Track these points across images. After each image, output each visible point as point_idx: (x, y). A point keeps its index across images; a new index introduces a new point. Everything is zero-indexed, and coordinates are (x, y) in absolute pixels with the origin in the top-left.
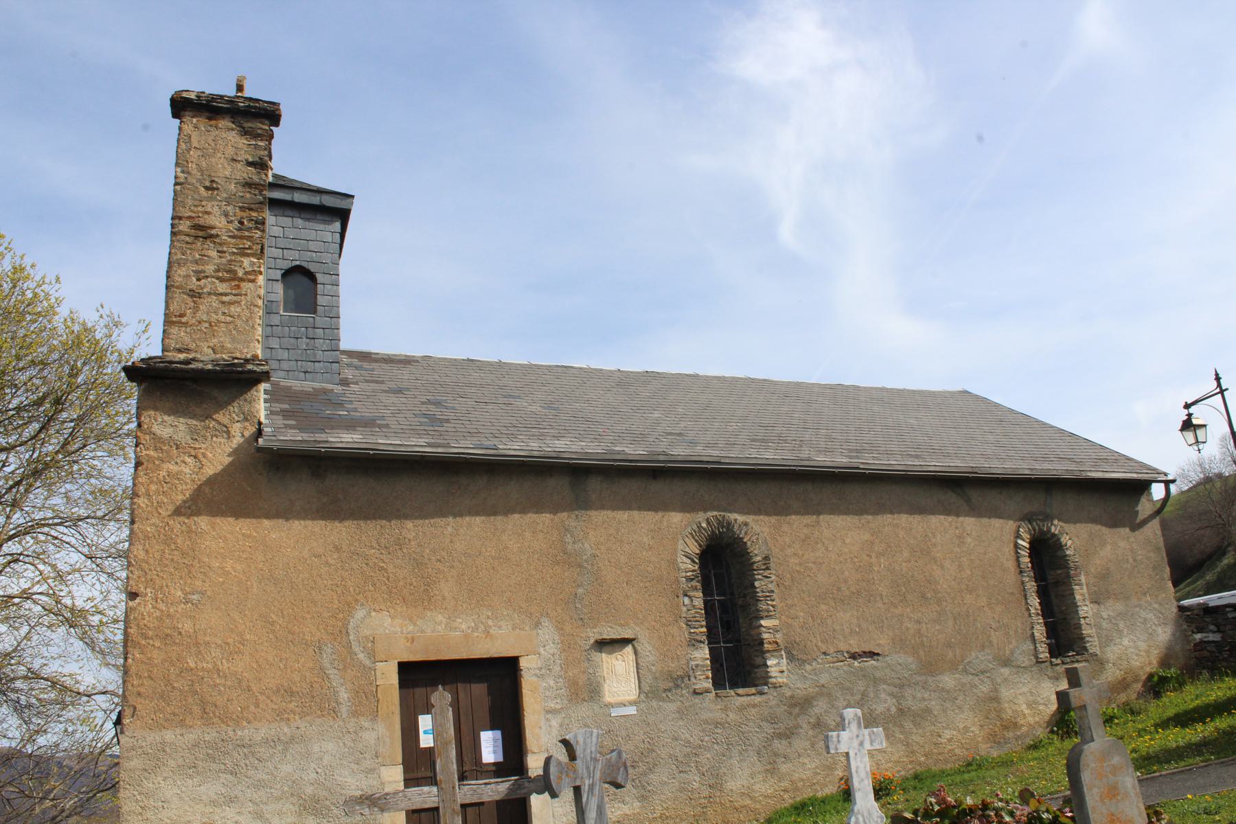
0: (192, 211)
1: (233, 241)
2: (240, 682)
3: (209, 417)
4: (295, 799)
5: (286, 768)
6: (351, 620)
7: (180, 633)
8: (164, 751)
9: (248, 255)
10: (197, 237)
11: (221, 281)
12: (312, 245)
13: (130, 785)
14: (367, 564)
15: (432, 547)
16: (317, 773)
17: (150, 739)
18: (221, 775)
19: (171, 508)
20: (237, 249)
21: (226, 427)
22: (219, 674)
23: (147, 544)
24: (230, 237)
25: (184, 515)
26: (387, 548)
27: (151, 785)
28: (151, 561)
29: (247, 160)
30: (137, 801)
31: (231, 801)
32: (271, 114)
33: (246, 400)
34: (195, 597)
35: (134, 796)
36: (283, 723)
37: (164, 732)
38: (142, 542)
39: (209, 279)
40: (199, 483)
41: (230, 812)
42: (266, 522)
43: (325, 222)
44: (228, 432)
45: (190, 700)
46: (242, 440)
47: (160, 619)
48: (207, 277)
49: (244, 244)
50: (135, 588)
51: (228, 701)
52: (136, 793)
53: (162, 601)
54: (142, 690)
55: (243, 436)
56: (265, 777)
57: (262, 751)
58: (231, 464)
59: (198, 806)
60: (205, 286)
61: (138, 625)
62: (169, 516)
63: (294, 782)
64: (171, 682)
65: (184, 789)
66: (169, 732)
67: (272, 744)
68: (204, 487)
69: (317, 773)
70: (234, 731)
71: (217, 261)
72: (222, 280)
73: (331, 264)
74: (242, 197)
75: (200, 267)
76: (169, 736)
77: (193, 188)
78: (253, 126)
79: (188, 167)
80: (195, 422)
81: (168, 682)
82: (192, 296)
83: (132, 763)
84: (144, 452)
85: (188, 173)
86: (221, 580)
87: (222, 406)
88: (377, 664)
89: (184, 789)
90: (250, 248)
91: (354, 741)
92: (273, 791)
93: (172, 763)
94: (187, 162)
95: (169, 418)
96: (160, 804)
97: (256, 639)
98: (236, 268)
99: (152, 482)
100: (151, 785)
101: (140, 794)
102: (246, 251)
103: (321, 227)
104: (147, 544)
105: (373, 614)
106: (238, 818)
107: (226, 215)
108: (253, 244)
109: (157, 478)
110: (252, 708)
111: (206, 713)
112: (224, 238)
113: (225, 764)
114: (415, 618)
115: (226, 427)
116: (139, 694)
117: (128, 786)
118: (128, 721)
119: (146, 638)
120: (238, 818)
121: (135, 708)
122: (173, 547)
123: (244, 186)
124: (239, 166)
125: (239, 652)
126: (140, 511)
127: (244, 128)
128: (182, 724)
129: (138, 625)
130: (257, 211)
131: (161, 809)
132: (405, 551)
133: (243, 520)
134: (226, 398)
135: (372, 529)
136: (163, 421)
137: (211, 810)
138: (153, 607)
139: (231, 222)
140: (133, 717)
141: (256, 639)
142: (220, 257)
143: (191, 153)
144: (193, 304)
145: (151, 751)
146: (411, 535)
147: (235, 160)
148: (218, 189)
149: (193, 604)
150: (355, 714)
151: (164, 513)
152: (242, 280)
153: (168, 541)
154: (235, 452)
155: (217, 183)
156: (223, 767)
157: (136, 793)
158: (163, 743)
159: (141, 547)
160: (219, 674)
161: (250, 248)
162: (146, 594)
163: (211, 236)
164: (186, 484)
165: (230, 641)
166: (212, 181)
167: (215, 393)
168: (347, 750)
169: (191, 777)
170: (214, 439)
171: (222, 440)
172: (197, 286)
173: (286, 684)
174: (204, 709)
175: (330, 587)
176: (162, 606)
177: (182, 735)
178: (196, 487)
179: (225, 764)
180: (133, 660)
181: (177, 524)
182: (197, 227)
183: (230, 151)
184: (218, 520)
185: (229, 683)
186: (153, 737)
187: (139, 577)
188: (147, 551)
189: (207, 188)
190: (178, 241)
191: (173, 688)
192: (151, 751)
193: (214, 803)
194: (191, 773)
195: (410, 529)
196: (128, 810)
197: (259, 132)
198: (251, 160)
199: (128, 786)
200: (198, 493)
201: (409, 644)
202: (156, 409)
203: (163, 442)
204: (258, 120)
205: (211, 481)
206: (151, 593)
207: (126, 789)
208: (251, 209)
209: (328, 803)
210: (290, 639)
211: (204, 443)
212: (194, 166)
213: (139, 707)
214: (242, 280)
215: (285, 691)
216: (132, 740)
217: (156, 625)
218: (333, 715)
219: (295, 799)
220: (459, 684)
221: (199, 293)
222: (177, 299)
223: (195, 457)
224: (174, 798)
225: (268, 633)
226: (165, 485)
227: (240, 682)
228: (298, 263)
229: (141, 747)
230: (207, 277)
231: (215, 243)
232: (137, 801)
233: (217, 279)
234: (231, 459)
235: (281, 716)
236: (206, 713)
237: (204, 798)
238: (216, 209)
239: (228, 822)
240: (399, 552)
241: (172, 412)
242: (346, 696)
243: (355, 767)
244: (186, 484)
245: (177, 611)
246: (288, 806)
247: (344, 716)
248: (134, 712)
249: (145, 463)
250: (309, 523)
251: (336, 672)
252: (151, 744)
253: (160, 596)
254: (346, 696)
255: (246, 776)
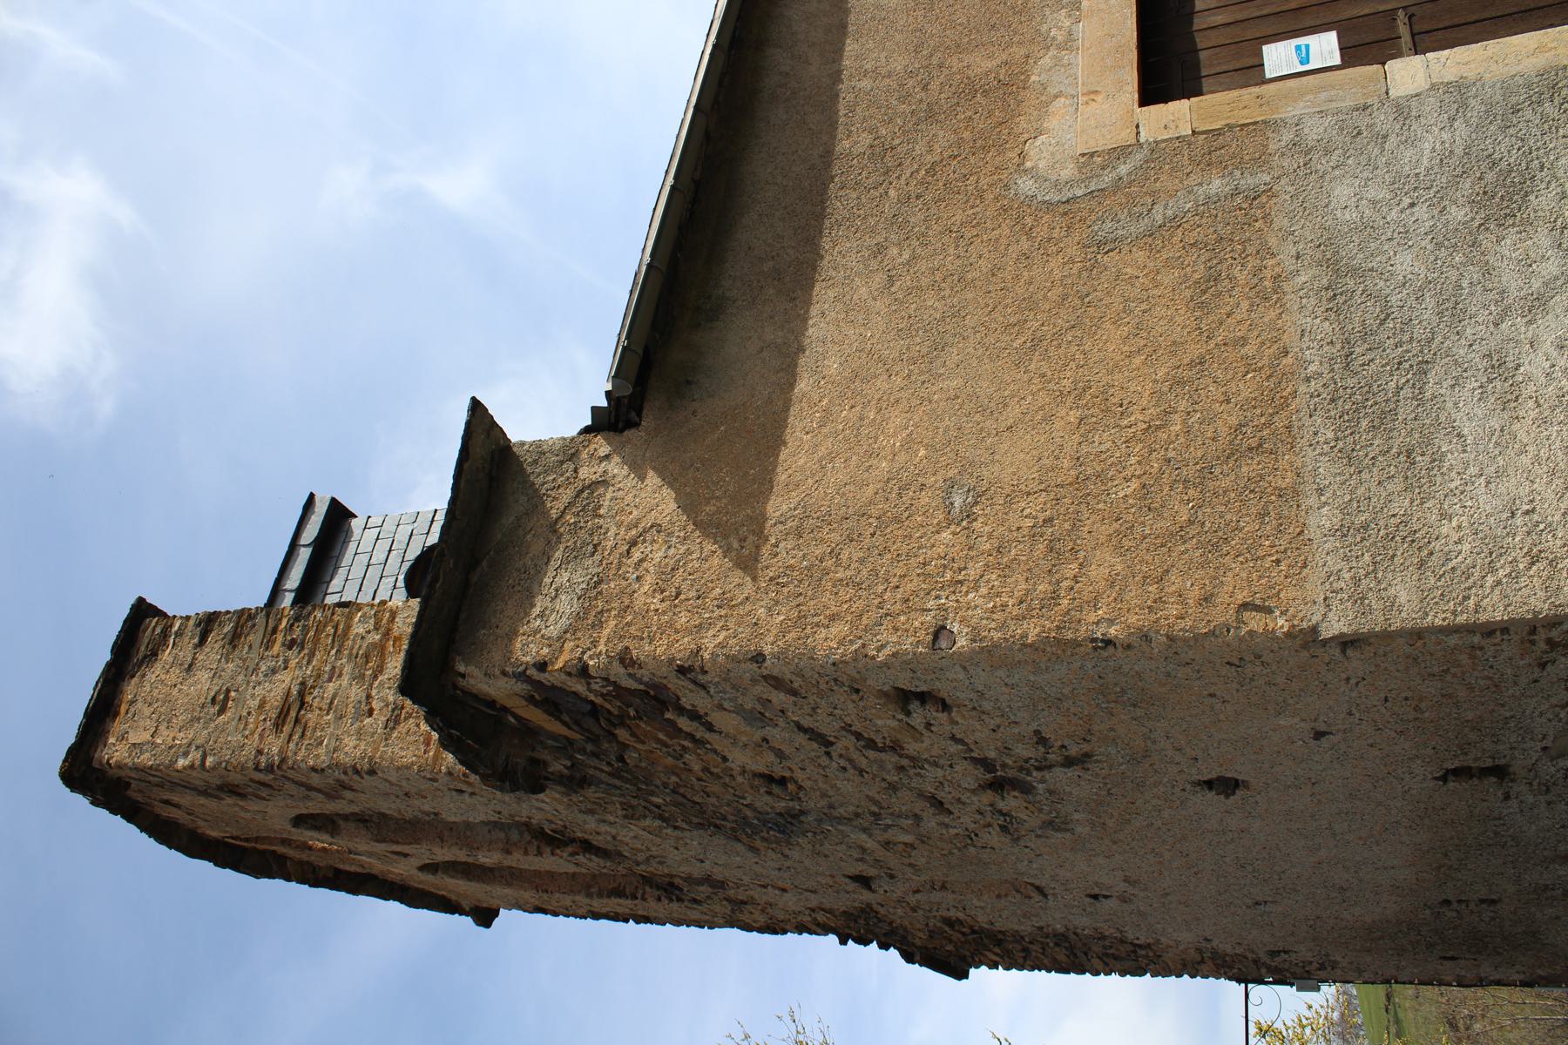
0: (252, 733)
1: (318, 655)
2: (1180, 383)
3: (553, 527)
4: (1486, 240)
5: (1405, 263)
6: (1039, 199)
7: (1049, 521)
8: (1365, 527)
9: (348, 627)
10: (297, 721)
11: (381, 672)
12: (379, 556)
13: (1466, 598)
14: (918, 197)
15: (895, 103)
16: (1412, 205)
17: (1334, 563)
18: (1428, 395)
19: (737, 576)
20: (332, 648)
21: (582, 491)
22: (1158, 428)
23: (816, 619)
24: (309, 662)
25: (758, 547)
26: (886, 173)
27: (1466, 547)
28: (858, 605)
29: (196, 646)
30: (1514, 576)
31: (1499, 366)
32: (142, 611)
33: (535, 462)
34: (958, 501)
35: (1499, 583)
36: (1286, 287)
37: (1312, 532)
38: (808, 630)
39: (374, 692)
40: (691, 527)
41: (1534, 365)
42: (802, 386)
43: (346, 542)
44: (594, 485)
45: (1226, 483)
46: (616, 459)
47: (1006, 571)
48: (369, 697)
49: (328, 635)
50: (921, 634)
51: (1228, 401)
52: (1490, 580)
53: (960, 570)
54: (1194, 594)
55: (607, 457)
56: (1430, 302)
57: (1363, 314)
58: (661, 473)
59: (1522, 435)
60: (382, 699)
61: (1020, 618)
62: (754, 579)
63: (1439, 245)
64: (1177, 528)
65: (1473, 470)
66: (1312, 521)
67: (1340, 300)
68: (703, 517)
69: (1412, 205)
70: (1308, 380)
71: (345, 681)
72: (380, 670)
73: (415, 525)
74: (250, 647)
75: (351, 710)
76: (1322, 519)
77: (216, 734)
78: (146, 641)
79: (180, 745)
80: (558, 554)
81: (1179, 534)
82: (397, 722)
83: (1403, 597)
84: (602, 648)
85: (190, 744)
86: (922, 453)
87: (536, 501)
88: (1142, 140)
89: (1473, 470)
90: (336, 628)
91: (1327, 152)
92: (1465, 284)
93: (1400, 505)
94: (171, 748)
95: (539, 604)
96: (1519, 521)
97: (1073, 365)
98: (365, 645)
99: (670, 624)
100: (1466, 547)
101: (1493, 571)
102: (340, 631)
103: (352, 547)
104: (816, 619)
105: (1028, 164)
106: (1547, 346)
107: (274, 671)
108: (331, 620)
109: (664, 613)
110: (1248, 350)
111: (1260, 445)
112: (308, 672)
113: (1399, 389)
114: (1043, 98)
115: (582, 491)
116: (1207, 599)
117: (1471, 602)
118: (1281, 622)
119: (1055, 596)
120: (1547, 346)
121: (1245, 606)
122: (829, 563)
123: (235, 647)
124: (200, 657)
125: (1105, 395)
126: (732, 642)
127: (145, 657)
128: (1291, 494)
129: (1020, 618)
130: (280, 620)
131: (1536, 517)
132: (897, 141)
133: (788, 431)
134: (523, 499)
135: (841, 202)
136: (541, 615)
137: (1531, 403)
138: (976, 588)
139: (286, 661)
140: (1269, 611)
141: (1073, 365)
142: (340, 675)
143: (159, 741)
144: (411, 720)
145: (1367, 557)
146: (866, 139)
147: (190, 666)
148: (228, 691)
149: (976, 503)
150: (1261, 160)
151: (749, 587)
152: (387, 634)
153: (815, 575)
154: (638, 470)
155: (217, 693)
156: (1406, 392)
157: (1490, 580)
158: (1342, 532)
159: (823, 633)
160: (1158, 428)
161: (336, 628)
162: (940, 608)
163: (301, 694)
164: (689, 552)
165: (1073, 416)
166: (214, 700)
167: (508, 520)
168: (1350, 162)
169: (1438, 459)
170: (602, 511)
171: (609, 496)
172: (380, 714)
173: (1188, 293)
174: (1250, 449)
175: (961, 251)
176: (973, 572)
177: (1320, 491)
178: (698, 533)
179: (1399, 389)
180: (1111, 622)
181: (781, 554)
182: (278, 725)
183: (175, 675)
184: (782, 477)
185: (1183, 405)
186: (1327, 556)
187: (896, 629)
188: (833, 618)
189: (222, 711)
190: (296, 753)
191: (1190, 522)
192: (1367, 557)
193: (1509, 401)
194: (1427, 458)
195: (852, 142)
196: (1541, 594)
197: (158, 630)
198: (196, 640)
199: (1471, 602)
200: (710, 528)
201: (1099, 98)
202: (514, 633)
203: (587, 611)
204: (141, 635)
205: (688, 505)
206: (938, 597)
207: (1477, 605)
208: (275, 630)
209: (1490, 177)
210: (1077, 302)
211: (608, 530)
212: (182, 735)
213: (1241, 597)
214: (387, 634)
215: (1204, 292)
216: (1335, 603)
217: (1021, 579)
218: (1264, 199)
219: (1486, 240)
220: (1195, 28)
221: (393, 710)
222: (396, 750)
223: (633, 543)
224: (1502, 489)
225: (1059, 346)
226: (682, 597)
227: (1180, 383)
228: (401, 577)
229: (1356, 581)
230: (369, 697)
231: (313, 687)
232: (1514, 576)
233: (376, 677)
234: (651, 473)
235: (1270, 293)
236: (1260, 445)
237: (1495, 423)
238: (259, 691)
239: (1562, 362)
240: (899, 149)
241: (528, 598)
242: (1217, 183)
243: (1393, 141)
244: (689, 552)
245: (990, 536)
246: (1506, 247)
247: (1268, 179)
248: (1258, 608)
249: (626, 643)
250: (814, 311)
251: (1159, 208)
252: (1346, 558)
253: (948, 575)
254: (1217, 183)
255: (1430, 341)
